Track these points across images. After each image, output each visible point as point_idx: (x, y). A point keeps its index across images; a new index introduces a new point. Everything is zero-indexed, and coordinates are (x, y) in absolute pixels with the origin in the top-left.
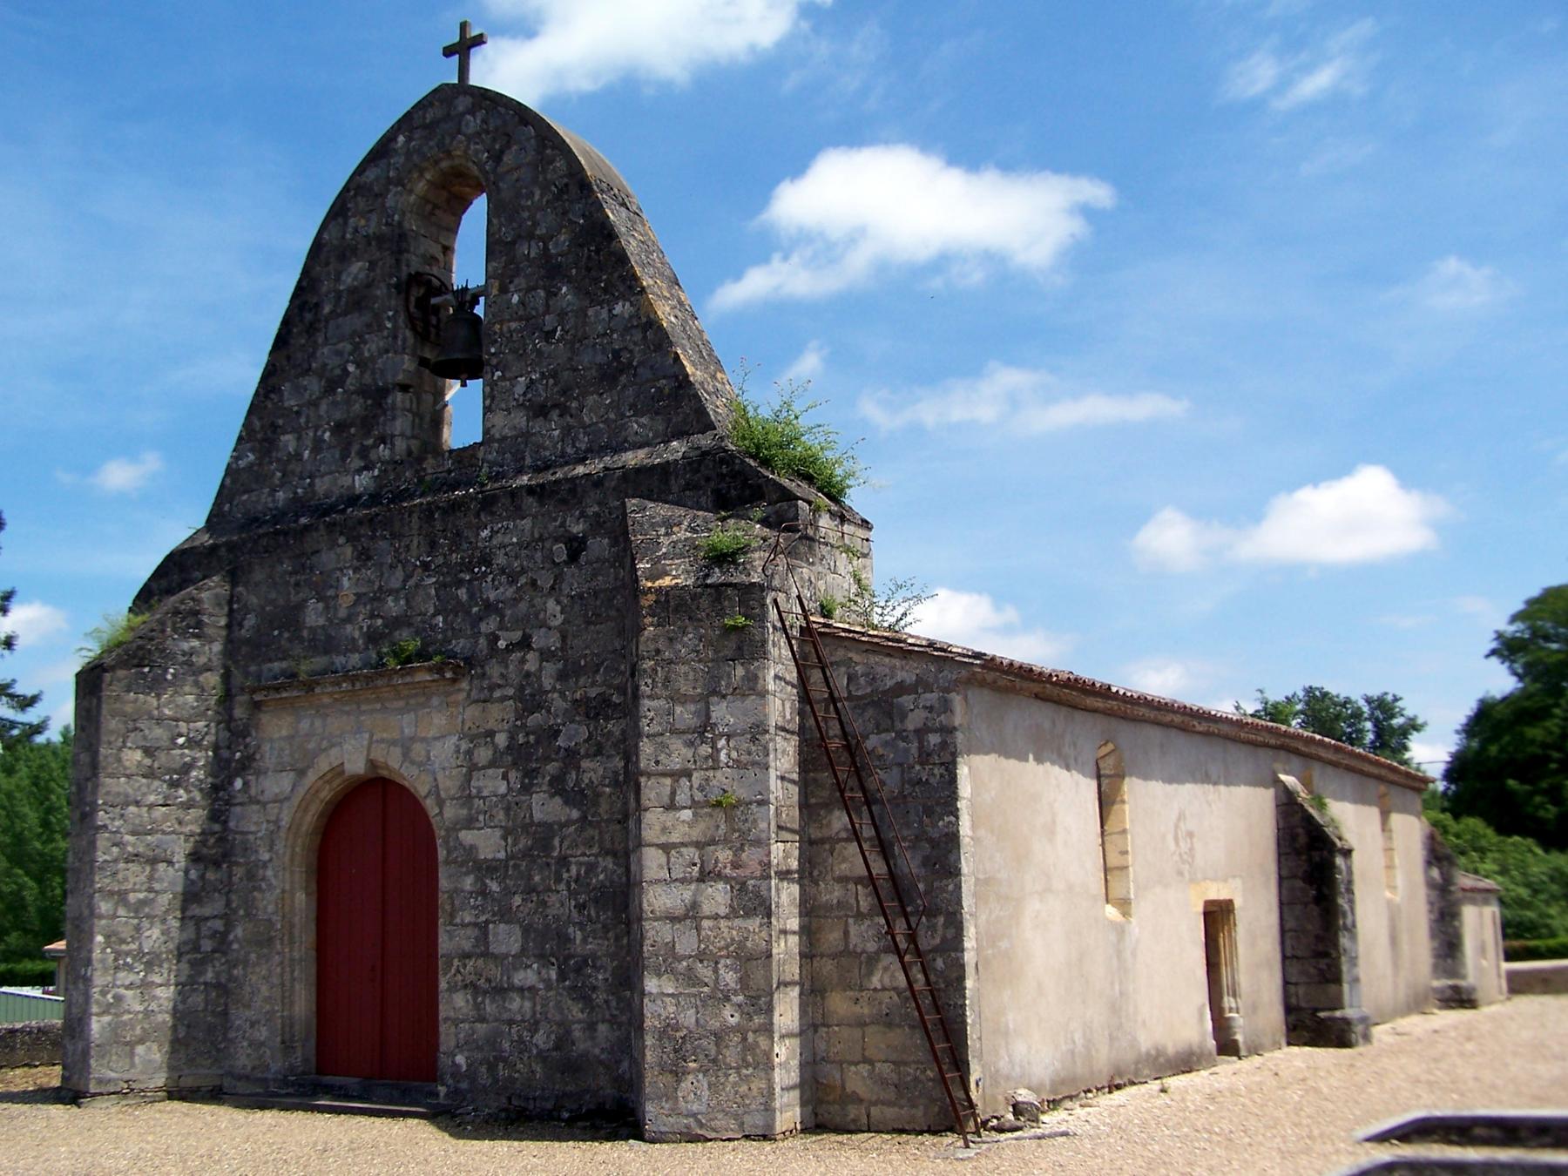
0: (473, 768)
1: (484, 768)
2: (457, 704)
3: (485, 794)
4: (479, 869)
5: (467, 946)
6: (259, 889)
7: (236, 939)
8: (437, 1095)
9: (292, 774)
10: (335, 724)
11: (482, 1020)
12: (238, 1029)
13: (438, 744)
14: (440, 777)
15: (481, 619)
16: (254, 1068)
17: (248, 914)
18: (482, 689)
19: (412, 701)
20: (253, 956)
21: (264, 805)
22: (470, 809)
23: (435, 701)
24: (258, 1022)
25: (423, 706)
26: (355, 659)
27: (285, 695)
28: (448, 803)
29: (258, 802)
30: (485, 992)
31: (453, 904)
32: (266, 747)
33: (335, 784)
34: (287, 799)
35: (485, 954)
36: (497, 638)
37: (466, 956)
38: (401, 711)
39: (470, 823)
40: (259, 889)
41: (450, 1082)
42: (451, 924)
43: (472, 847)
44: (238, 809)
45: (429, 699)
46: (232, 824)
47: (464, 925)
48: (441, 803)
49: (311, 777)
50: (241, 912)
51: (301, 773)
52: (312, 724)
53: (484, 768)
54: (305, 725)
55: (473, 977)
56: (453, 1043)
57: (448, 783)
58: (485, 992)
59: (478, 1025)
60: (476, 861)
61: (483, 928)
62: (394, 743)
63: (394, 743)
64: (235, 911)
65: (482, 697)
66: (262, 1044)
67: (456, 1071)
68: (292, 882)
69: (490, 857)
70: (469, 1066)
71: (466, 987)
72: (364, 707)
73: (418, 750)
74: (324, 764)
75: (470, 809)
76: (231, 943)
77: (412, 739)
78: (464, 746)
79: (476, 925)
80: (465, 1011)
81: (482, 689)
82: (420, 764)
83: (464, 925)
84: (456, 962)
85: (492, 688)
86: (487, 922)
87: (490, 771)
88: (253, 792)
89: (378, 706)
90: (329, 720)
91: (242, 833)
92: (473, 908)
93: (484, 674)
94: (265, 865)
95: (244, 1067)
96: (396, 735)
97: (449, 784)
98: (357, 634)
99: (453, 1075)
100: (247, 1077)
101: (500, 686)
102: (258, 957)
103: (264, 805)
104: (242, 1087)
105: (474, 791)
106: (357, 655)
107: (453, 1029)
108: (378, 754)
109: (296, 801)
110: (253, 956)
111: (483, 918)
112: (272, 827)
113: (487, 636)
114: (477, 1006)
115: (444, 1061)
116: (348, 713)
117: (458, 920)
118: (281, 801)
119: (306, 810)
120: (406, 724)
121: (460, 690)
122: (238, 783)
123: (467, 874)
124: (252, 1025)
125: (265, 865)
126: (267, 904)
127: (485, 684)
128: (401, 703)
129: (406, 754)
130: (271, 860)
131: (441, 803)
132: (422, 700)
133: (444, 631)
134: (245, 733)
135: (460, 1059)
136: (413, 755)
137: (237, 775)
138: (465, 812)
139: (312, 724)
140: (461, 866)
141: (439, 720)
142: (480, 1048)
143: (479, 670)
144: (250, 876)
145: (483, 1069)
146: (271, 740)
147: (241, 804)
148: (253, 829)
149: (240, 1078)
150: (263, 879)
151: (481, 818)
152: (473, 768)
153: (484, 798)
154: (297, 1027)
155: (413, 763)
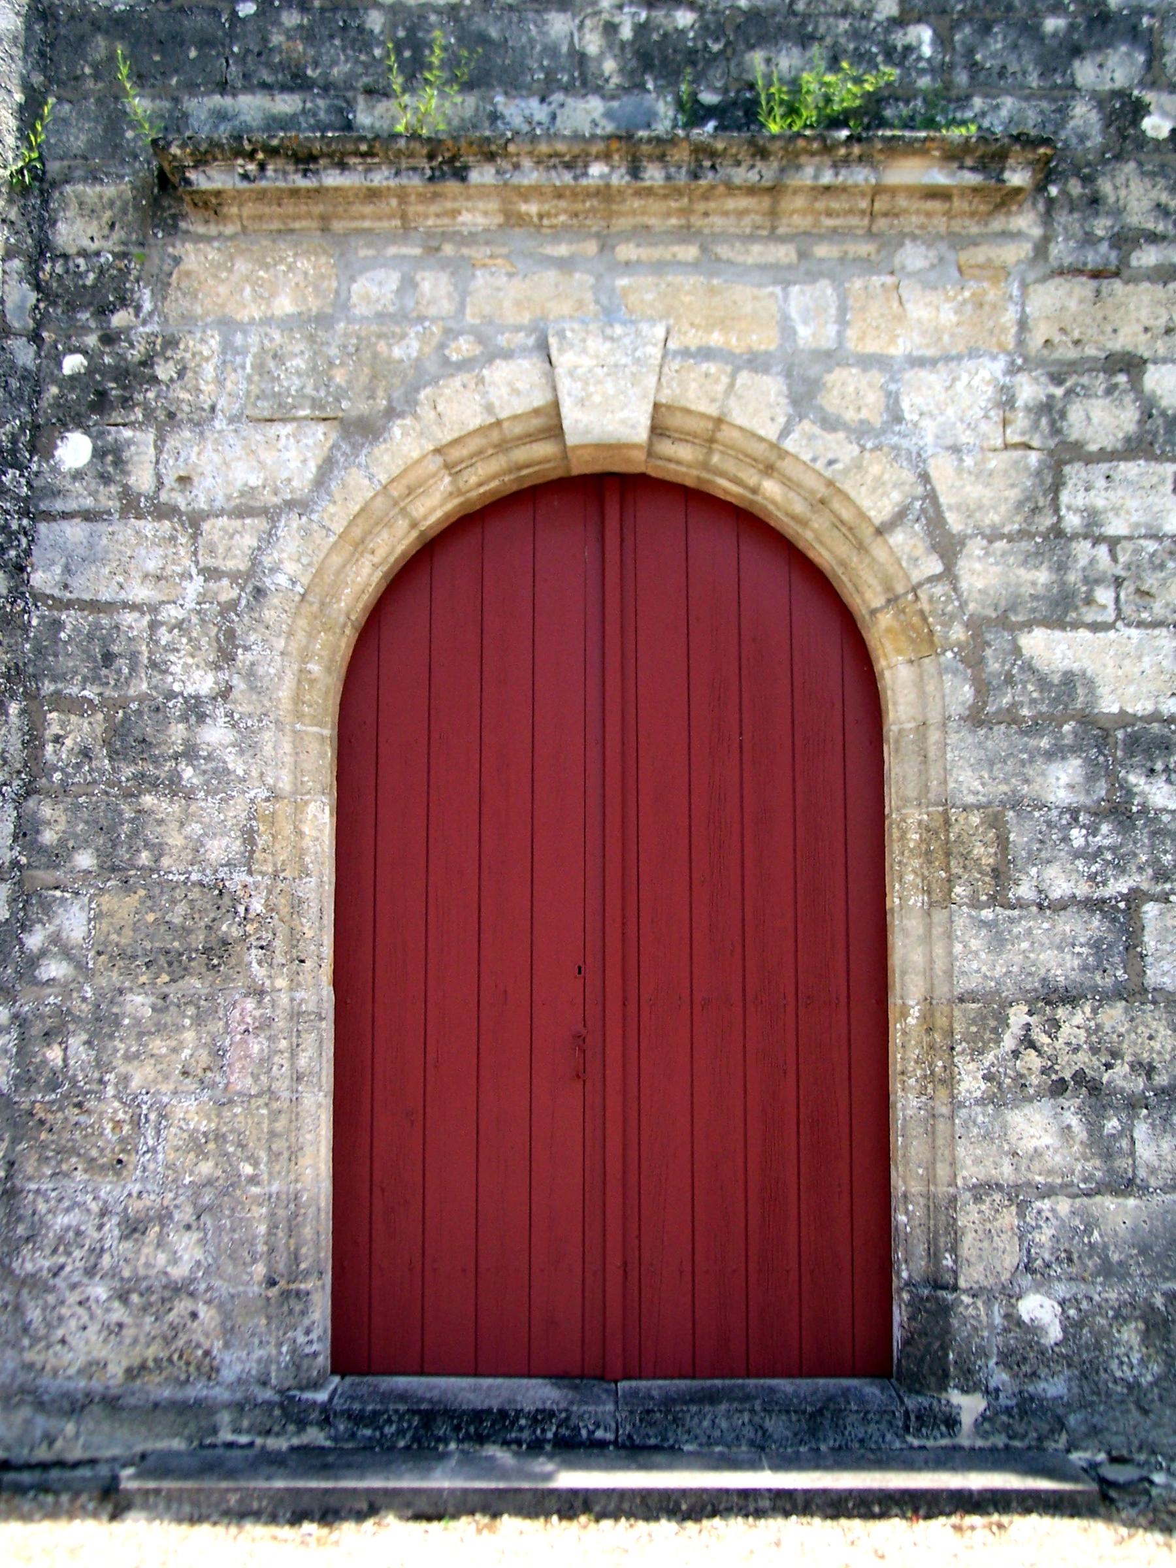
0: (1063, 455)
1: (1104, 456)
2: (1000, 273)
3: (1116, 527)
4: (1103, 739)
5: (1061, 967)
6: (173, 787)
7: (60, 946)
8: (951, 1422)
9: (319, 436)
10: (505, 291)
11: (1126, 1186)
12: (62, 1244)
13: (933, 379)
14: (942, 469)
15: (1077, 52)
16: (131, 1373)
17: (109, 867)
18: (1089, 240)
19: (822, 251)
20: (139, 1004)
21: (195, 521)
22: (1061, 568)
23: (913, 257)
24: (164, 1217)
25: (868, 266)
26: (586, 113)
27: (333, 179)
28: (975, 547)
29: (163, 512)
30: (1133, 1104)
31: (1003, 842)
32: (204, 346)
33: (471, 478)
34: (300, 506)
35: (1133, 992)
36: (1139, 110)
37: (1053, 997)
38: (782, 276)
39: (1061, 609)
40: (173, 787)
41: (1000, 1377)
42: (997, 899)
43: (1069, 680)
44: (74, 531)
45: (891, 243)
46: (41, 579)
47: (1046, 906)
48: (948, 548)
49: (404, 445)
50: (85, 860)
51: (363, 431)
52: (409, 284)
53: (1104, 456)
54: (375, 288)
55: (1083, 1059)
56: (1011, 1258)
57: (974, 491)
58: (1133, 1104)
59: (1109, 1203)
60: (1087, 720)
61: (1124, 917)
62: (756, 362)
63: (756, 362)
64: (57, 856)
65: (1092, 258)
66: (178, 1289)
67: (1023, 1351)
68: (297, 770)
69: (1142, 707)
70: (1071, 1328)
71: (1059, 1088)
72: (627, 251)
73: (852, 392)
74: (458, 409)
75: (1061, 568)
76: (34, 961)
77: (831, 357)
78: (1029, 390)
79: (1093, 905)
80: (1057, 1160)
81: (1089, 240)
82: (860, 432)
83: (1046, 906)
84: (1018, 1016)
85: (1126, 240)
86: (1135, 898)
87: (1129, 469)
88: (142, 479)
89: (689, 252)
90: (481, 278)
91: (94, 606)
92: (1078, 854)
93: (1094, 201)
94: (196, 710)
95: (94, 1367)
96: (764, 340)
97: (982, 488)
98: (593, 43)
99: (1007, 1358)
100: (111, 1403)
101: (1154, 238)
102: (163, 1002)
103: (195, 521)
104: (107, 1440)
105: (1072, 521)
106: (595, 105)
107: (1009, 1218)
108: (698, 392)
109: (336, 514)
110: (139, 1004)
111: (1119, 886)
112: (226, 591)
113: (1100, 101)
114: (1103, 1147)
115: (974, 1316)
116: (565, 265)
117: (1025, 891)
118: (271, 514)
119: (360, 546)
120: (809, 313)
121: (1007, 235)
122: (75, 450)
123: (1057, 753)
124: (133, 1228)
125: (196, 710)
126: (195, 835)
127: (1101, 226)
128: (784, 253)
129: (804, 397)
130: (225, 693)
131: (948, 548)
132: (865, 248)
133: (940, 70)
134: (108, 295)
135: (1039, 1309)
136: (830, 401)
137: (71, 417)
138: (1043, 576)
139: (409, 284)
140: (1034, 728)
141: (927, 312)
142: (1109, 1271)
143: (1075, 188)
144: (127, 739)
145: (1130, 1334)
146: (227, 325)
147: (88, 516)
148: (140, 593)
149: (75, 1406)
150: (190, 753)
151: (1105, 595)
152: (1063, 455)
153: (1113, 543)
154: (308, 1232)
155: (830, 423)
